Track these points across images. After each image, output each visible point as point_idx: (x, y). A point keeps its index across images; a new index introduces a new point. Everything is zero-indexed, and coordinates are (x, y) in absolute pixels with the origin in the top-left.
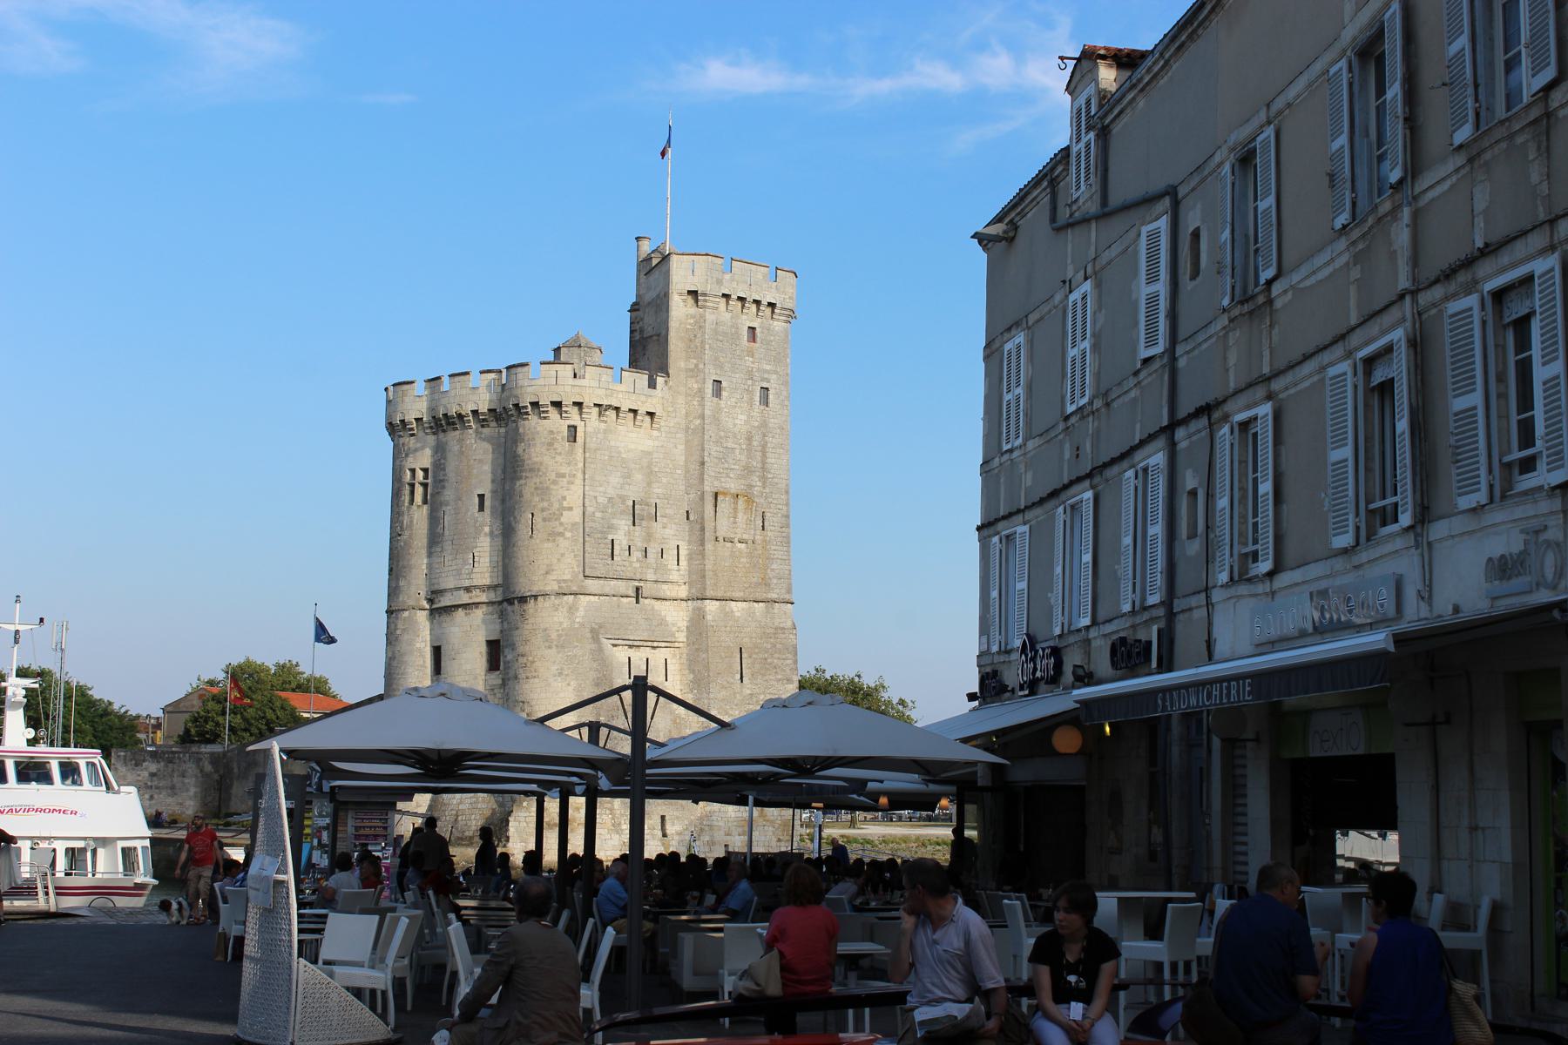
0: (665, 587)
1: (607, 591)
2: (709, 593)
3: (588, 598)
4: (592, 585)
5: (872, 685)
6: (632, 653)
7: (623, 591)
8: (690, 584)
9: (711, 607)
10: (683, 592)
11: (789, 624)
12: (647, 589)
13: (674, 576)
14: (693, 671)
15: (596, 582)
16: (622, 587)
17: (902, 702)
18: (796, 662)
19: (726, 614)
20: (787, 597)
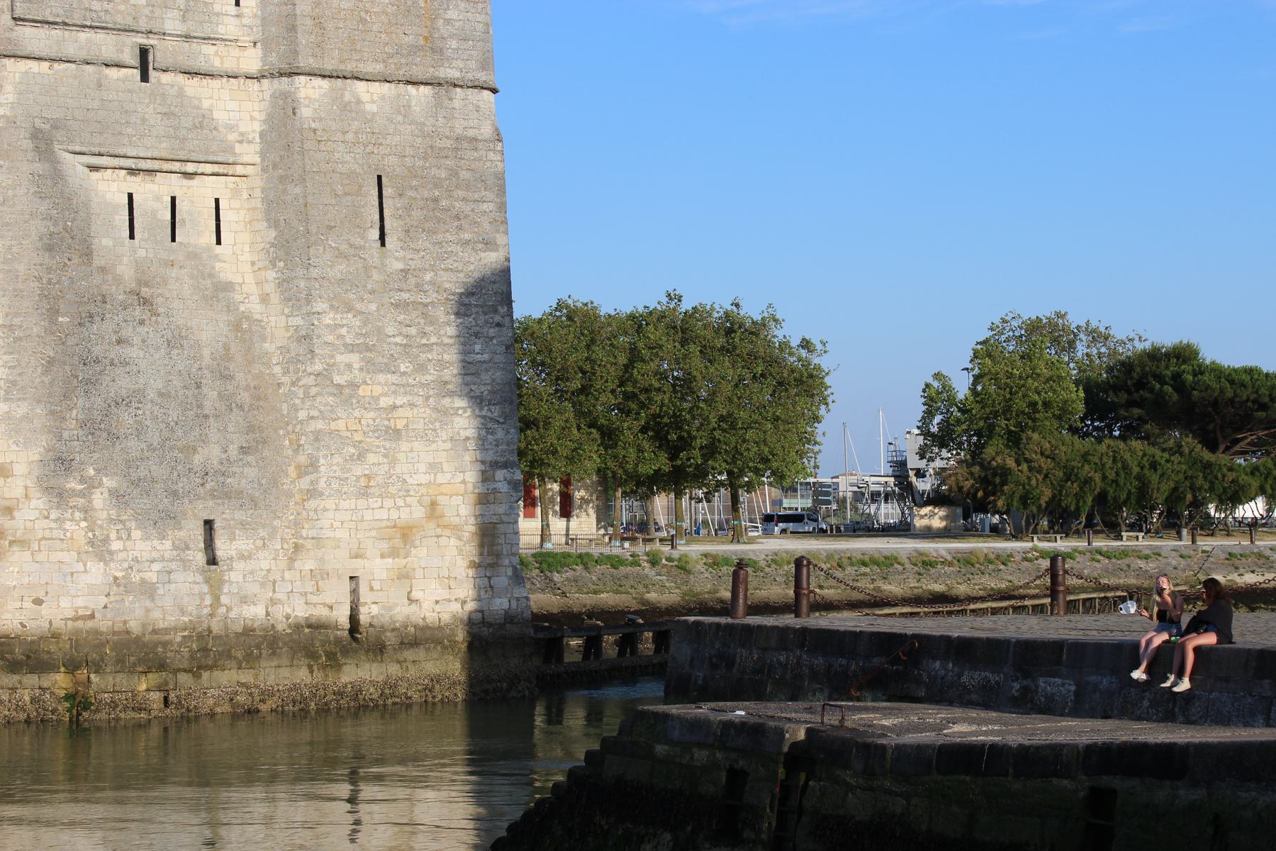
0: (208, 49)
1: (71, 51)
2: (305, 62)
3: (24, 65)
4: (33, 38)
5: (757, 317)
6: (137, 185)
7: (109, 53)
8: (265, 43)
9: (310, 91)
10: (252, 61)
11: (486, 131)
12: (163, 52)
13: (229, 27)
14: (275, 224)
15: (43, 32)
16: (106, 45)
17: (806, 344)
18: (502, 207)
19: (345, 107)
20: (482, 77)
